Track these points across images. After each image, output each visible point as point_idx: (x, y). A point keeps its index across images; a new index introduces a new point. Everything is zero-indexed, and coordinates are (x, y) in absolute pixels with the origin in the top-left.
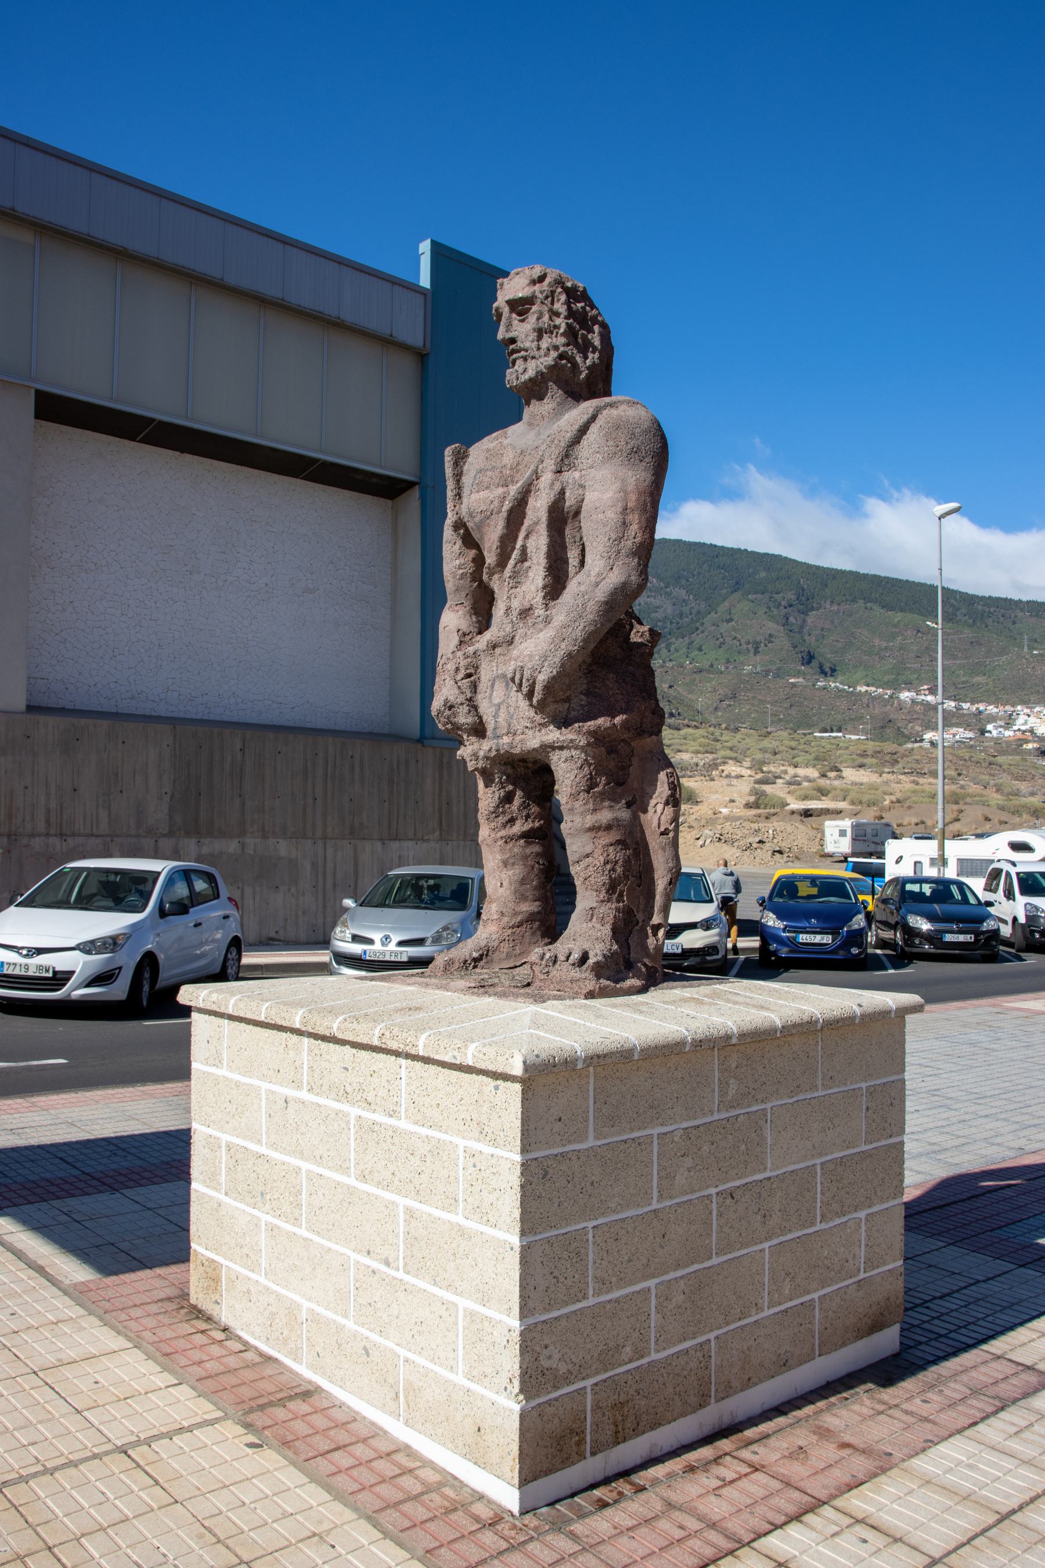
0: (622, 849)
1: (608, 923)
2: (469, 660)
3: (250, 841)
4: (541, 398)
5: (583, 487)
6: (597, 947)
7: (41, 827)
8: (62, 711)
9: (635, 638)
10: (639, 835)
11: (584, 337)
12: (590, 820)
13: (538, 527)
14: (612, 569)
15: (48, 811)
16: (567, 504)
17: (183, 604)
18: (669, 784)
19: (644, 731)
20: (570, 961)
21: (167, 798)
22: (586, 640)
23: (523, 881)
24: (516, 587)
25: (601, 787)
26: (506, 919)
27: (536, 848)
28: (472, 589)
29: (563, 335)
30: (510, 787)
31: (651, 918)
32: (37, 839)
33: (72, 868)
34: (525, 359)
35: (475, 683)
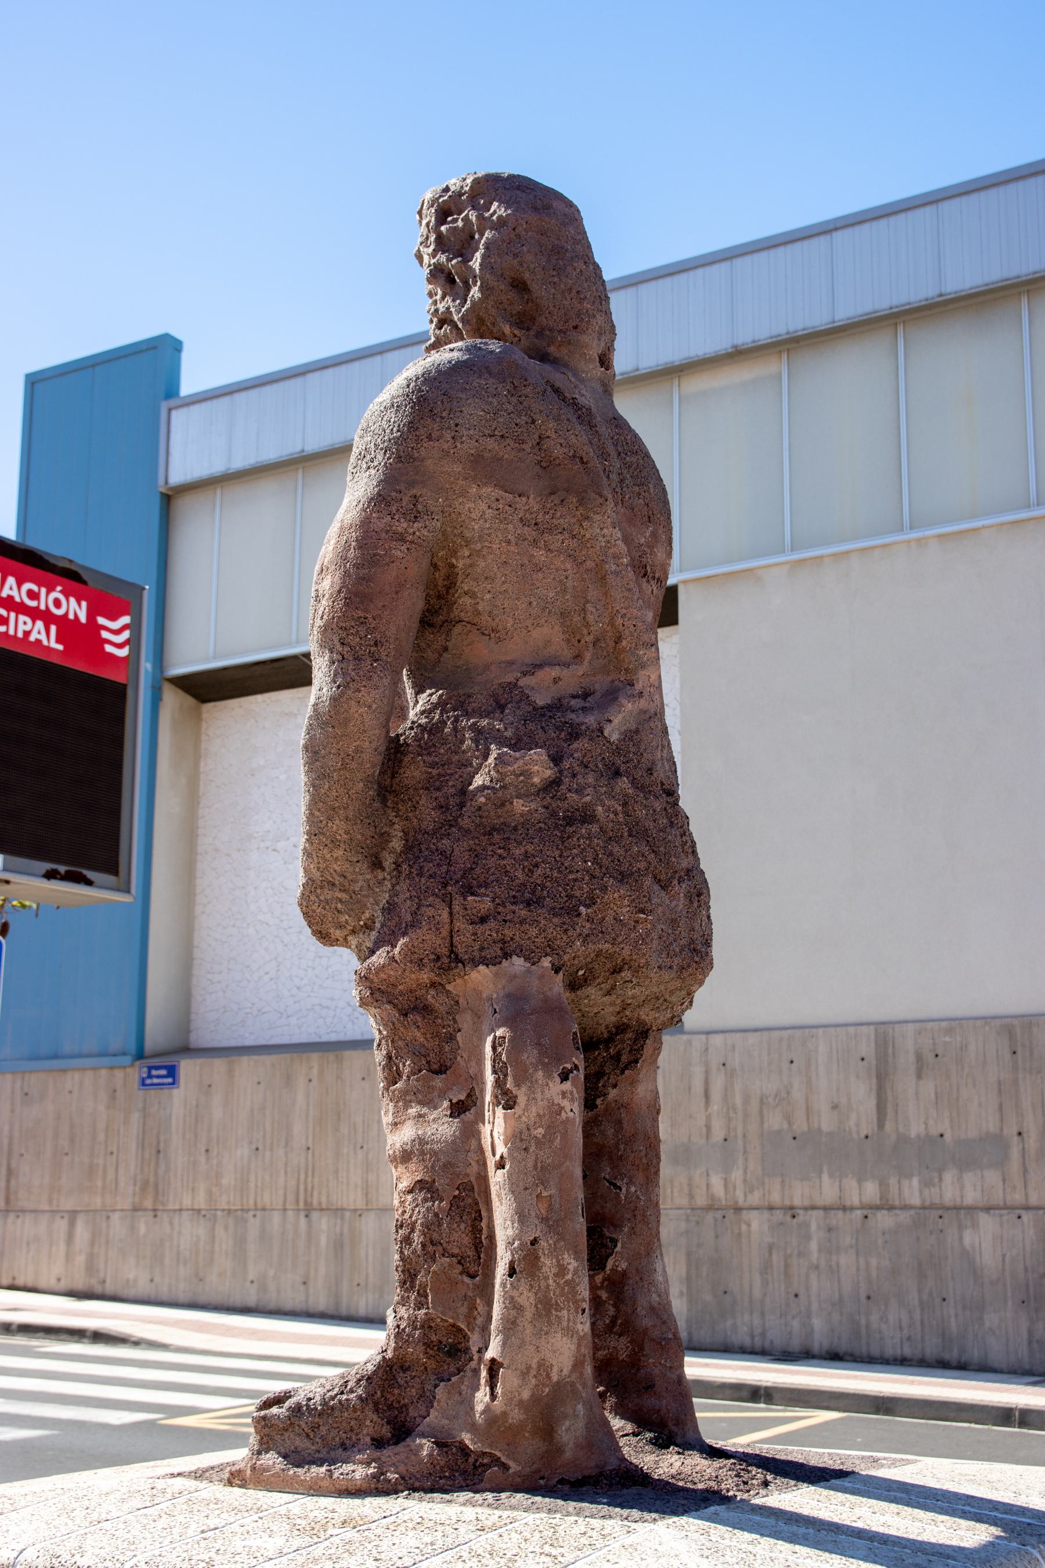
0: (425, 1200)
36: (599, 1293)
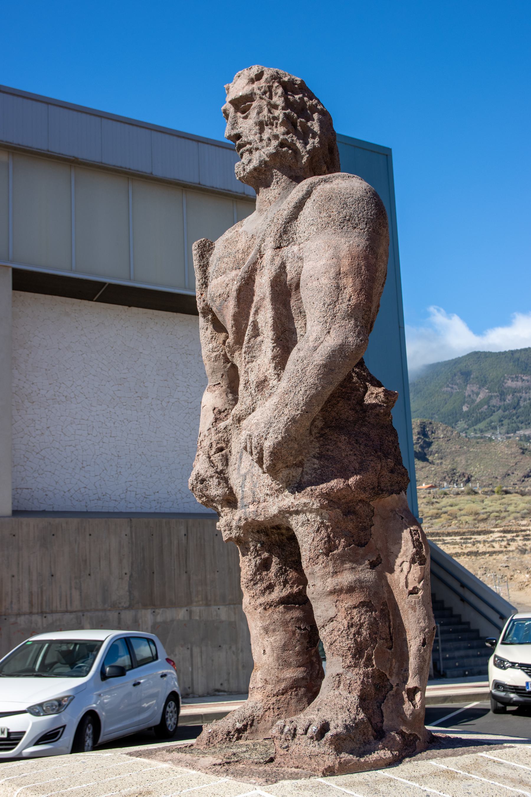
0: (366, 611)
1: (355, 689)
2: (220, 435)
3: (196, 609)
4: (267, 186)
5: (301, 259)
6: (340, 717)
7: (26, 607)
8: (43, 513)
9: (369, 400)
10: (386, 595)
11: (303, 125)
12: (331, 583)
13: (265, 302)
14: (329, 332)
15: (31, 594)
16: (289, 277)
17: (136, 422)
18: (413, 541)
19: (382, 491)
20: (309, 734)
21: (127, 578)
22: (309, 403)
23: (285, 648)
24: (252, 362)
25: (340, 549)
26: (269, 687)
27: (297, 614)
28: (226, 369)
29: (282, 124)
30: (266, 555)
31: (405, 682)
32: (23, 618)
33: (35, 642)
34: (250, 151)
35: (227, 456)
36: (312, 658)
